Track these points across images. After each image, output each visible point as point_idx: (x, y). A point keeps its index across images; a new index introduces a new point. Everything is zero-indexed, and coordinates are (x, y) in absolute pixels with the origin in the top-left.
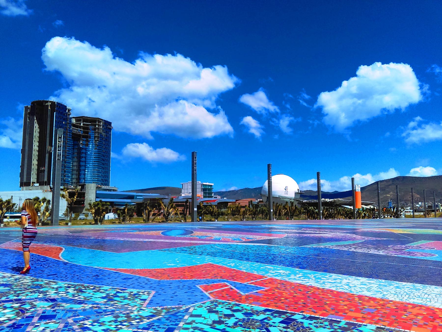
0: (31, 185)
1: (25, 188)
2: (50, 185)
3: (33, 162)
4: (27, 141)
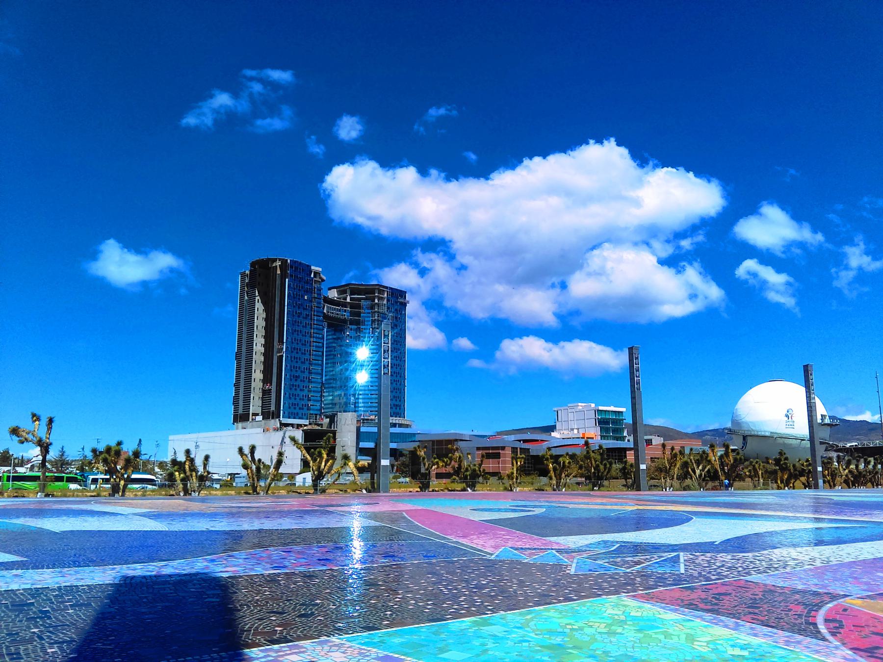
0: (250, 420)
1: (240, 425)
2: (280, 418)
3: (254, 376)
4: (245, 336)
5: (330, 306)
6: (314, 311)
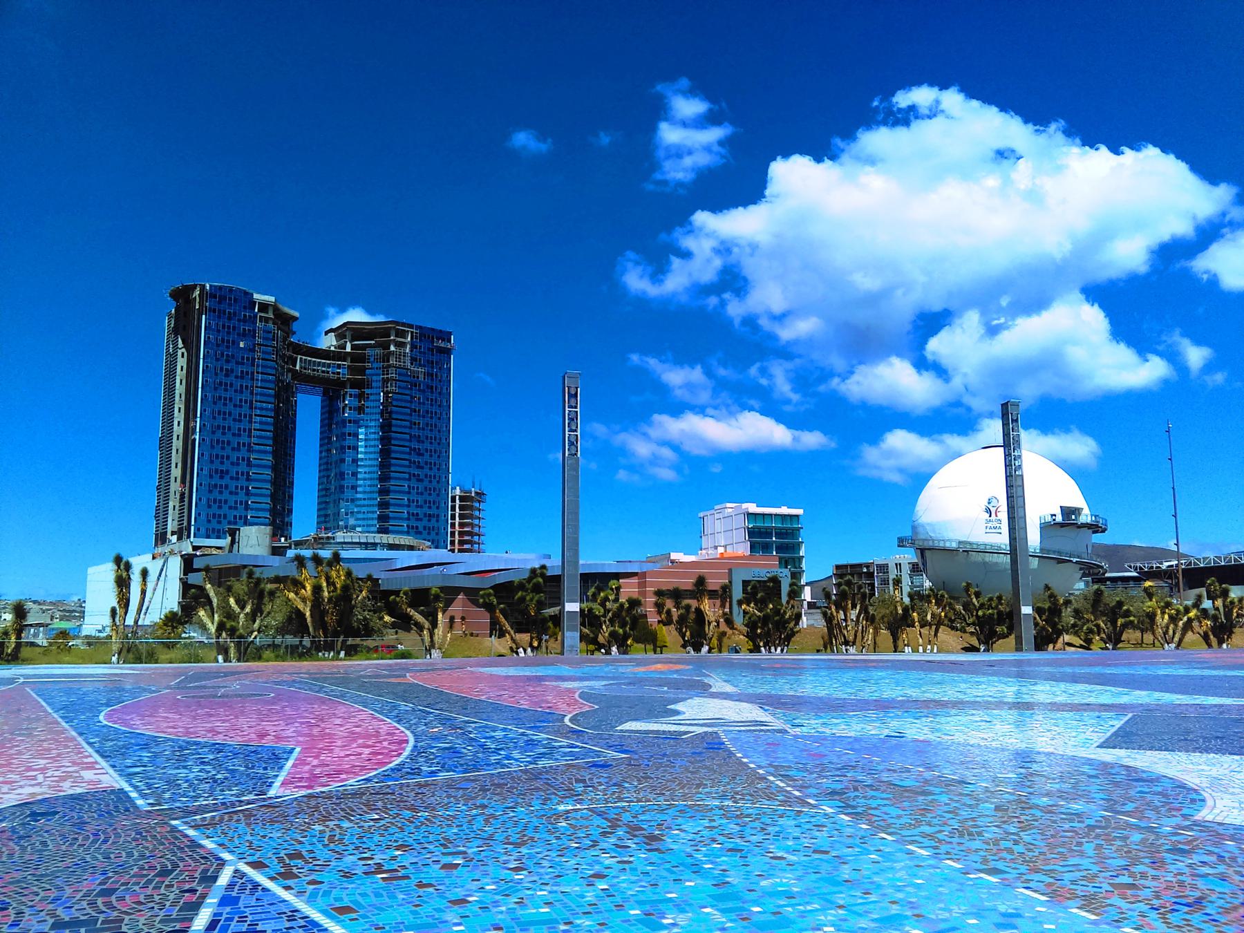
5: (314, 359)
6: (258, 366)
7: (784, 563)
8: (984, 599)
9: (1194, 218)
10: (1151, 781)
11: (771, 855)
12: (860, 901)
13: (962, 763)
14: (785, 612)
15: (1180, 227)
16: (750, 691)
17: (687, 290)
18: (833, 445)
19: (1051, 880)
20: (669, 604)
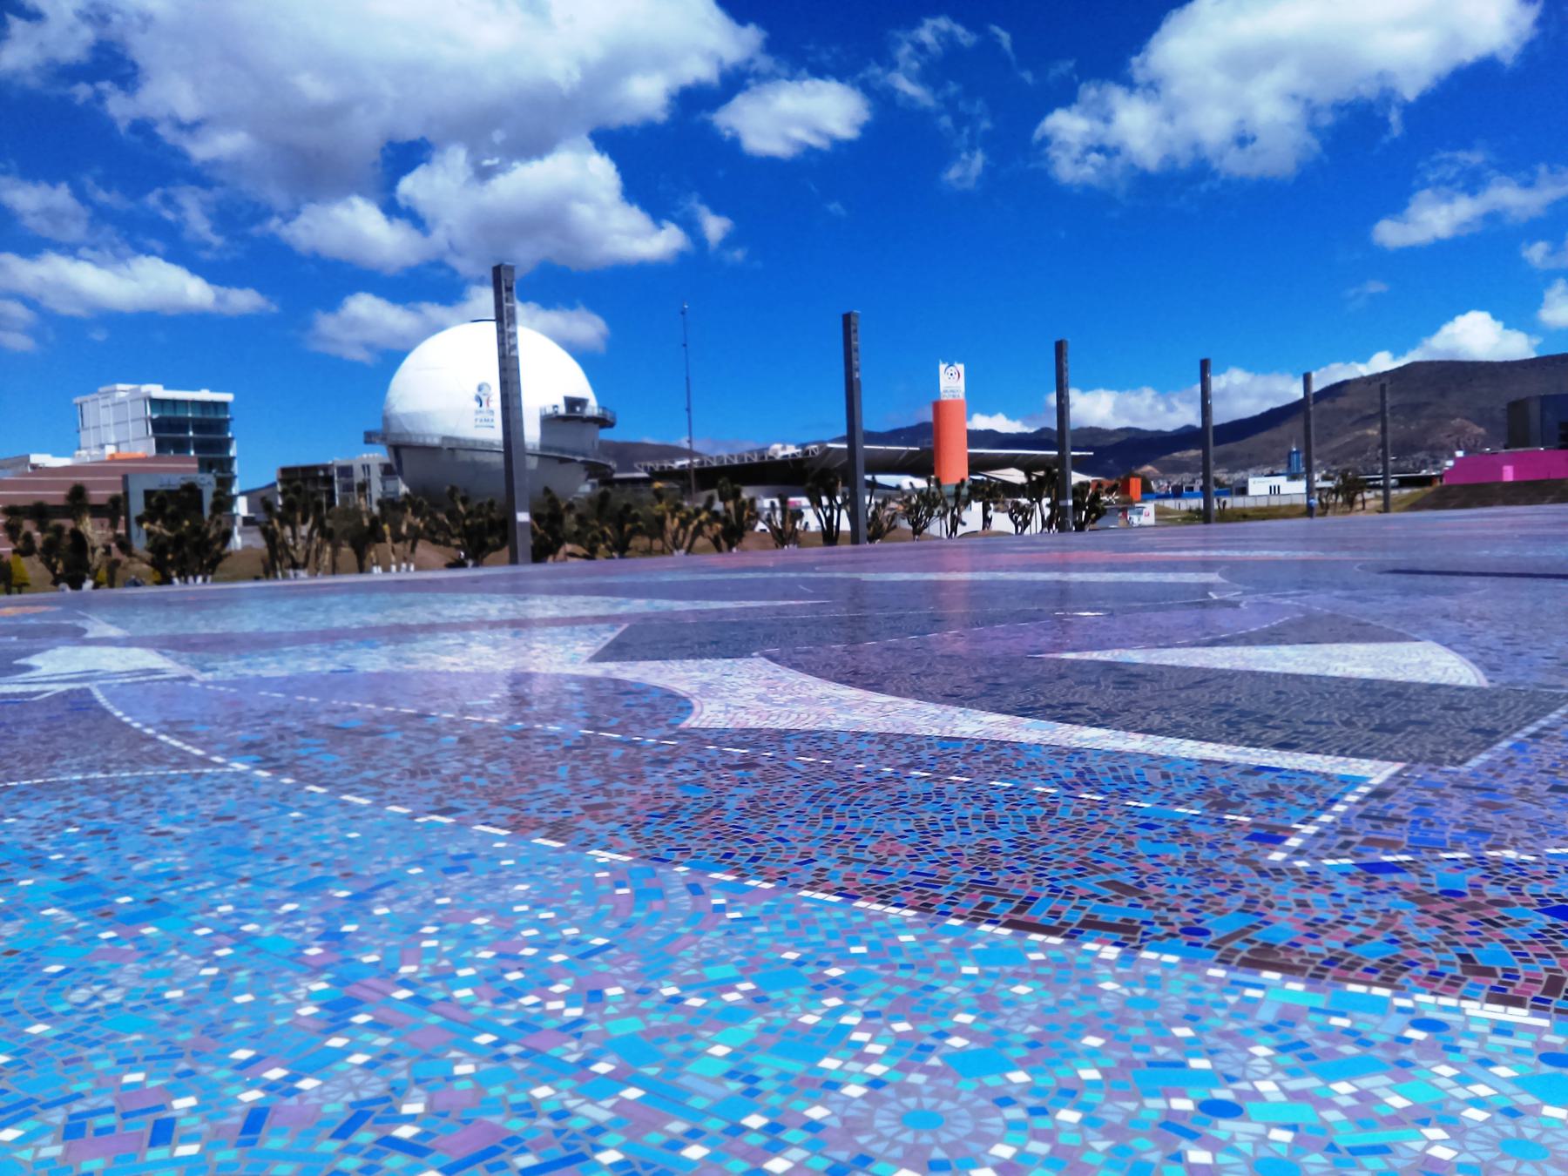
0: (1534, 409)
7: (206, 466)
8: (473, 505)
9: (720, 62)
10: (639, 693)
11: (152, 831)
12: (272, 869)
13: (425, 694)
14: (208, 531)
15: (699, 70)
16: (147, 633)
17: (37, 69)
18: (274, 309)
19: (516, 811)
20: (28, 526)
